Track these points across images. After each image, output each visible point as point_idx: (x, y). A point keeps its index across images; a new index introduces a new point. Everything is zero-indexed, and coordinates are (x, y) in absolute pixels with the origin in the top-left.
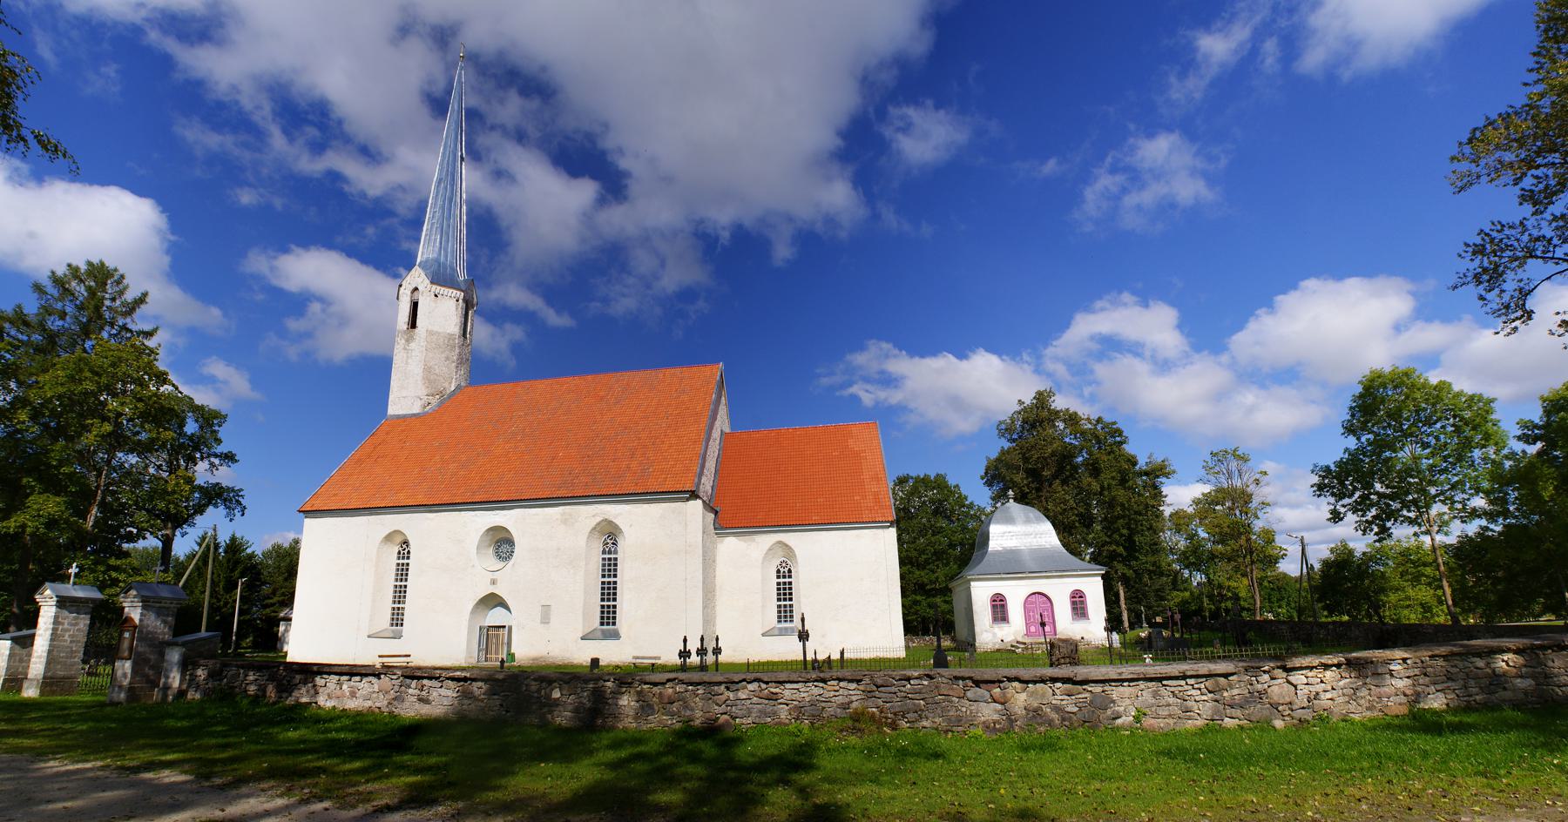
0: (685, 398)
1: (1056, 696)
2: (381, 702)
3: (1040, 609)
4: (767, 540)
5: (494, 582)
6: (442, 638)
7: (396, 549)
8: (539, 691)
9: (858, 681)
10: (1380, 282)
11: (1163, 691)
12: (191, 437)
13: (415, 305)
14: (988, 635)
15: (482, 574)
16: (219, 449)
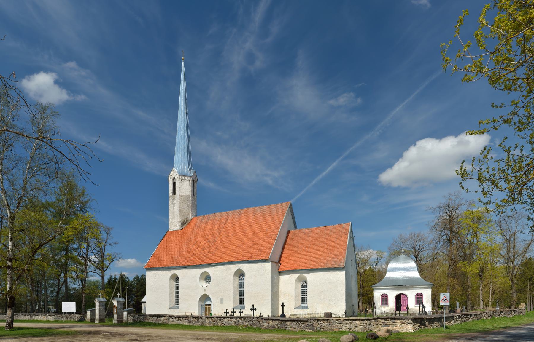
13: (174, 184)
14: (380, 309)
15: (202, 287)
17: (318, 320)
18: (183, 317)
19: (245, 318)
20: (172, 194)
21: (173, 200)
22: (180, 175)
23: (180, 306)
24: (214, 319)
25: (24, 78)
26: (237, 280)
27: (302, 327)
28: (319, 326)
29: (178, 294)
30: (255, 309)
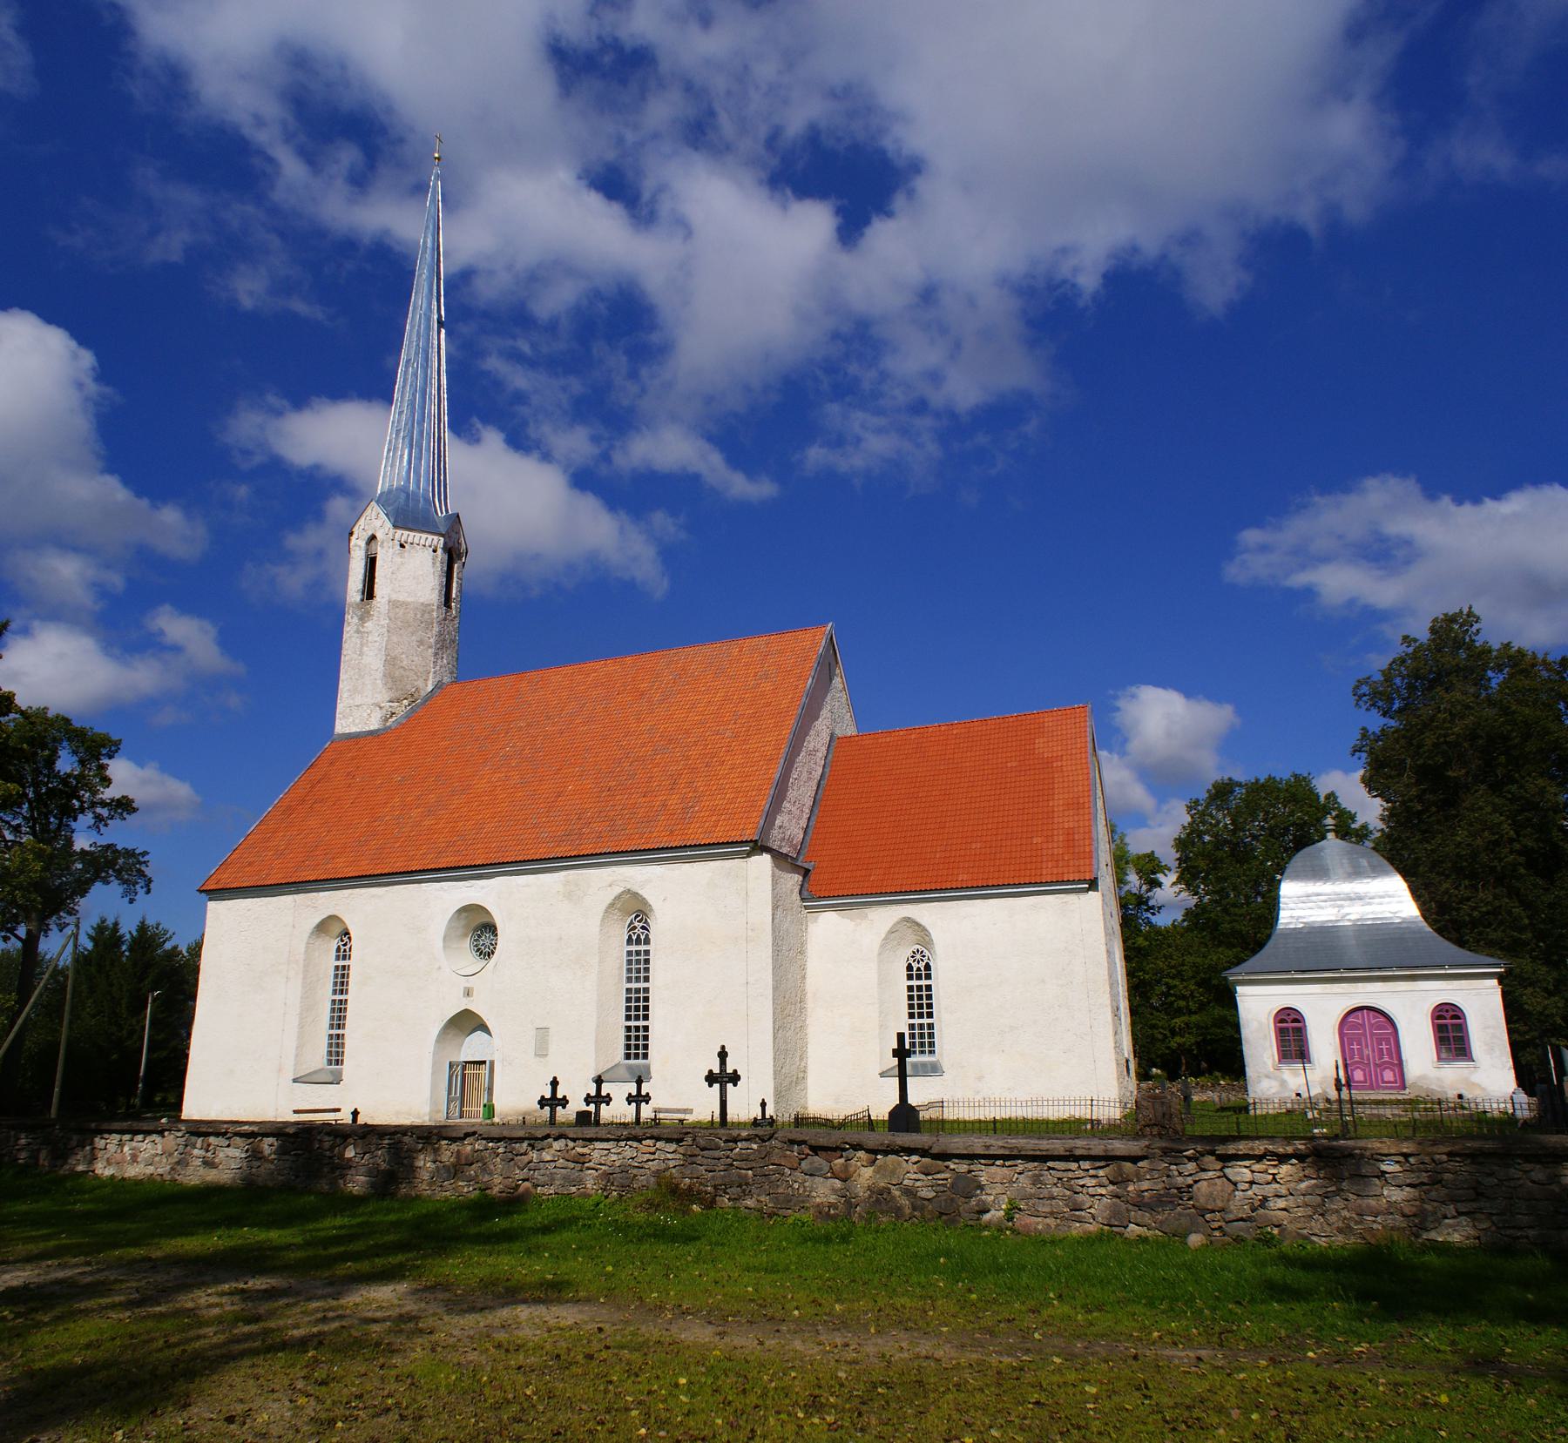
0: (767, 686)
1: (909, 1170)
2: (162, 1168)
3: (1369, 1032)
4: (884, 917)
5: (468, 993)
7: (335, 943)
8: (332, 1148)
9: (679, 1141)
11: (1049, 1178)
12: (65, 780)
13: (371, 563)
14: (1271, 1081)
15: (452, 979)
16: (108, 794)
17: (454, 1140)
20: (358, 598)
21: (363, 619)
23: (347, 1068)
25: (1374, 475)
30: (735, 1078)
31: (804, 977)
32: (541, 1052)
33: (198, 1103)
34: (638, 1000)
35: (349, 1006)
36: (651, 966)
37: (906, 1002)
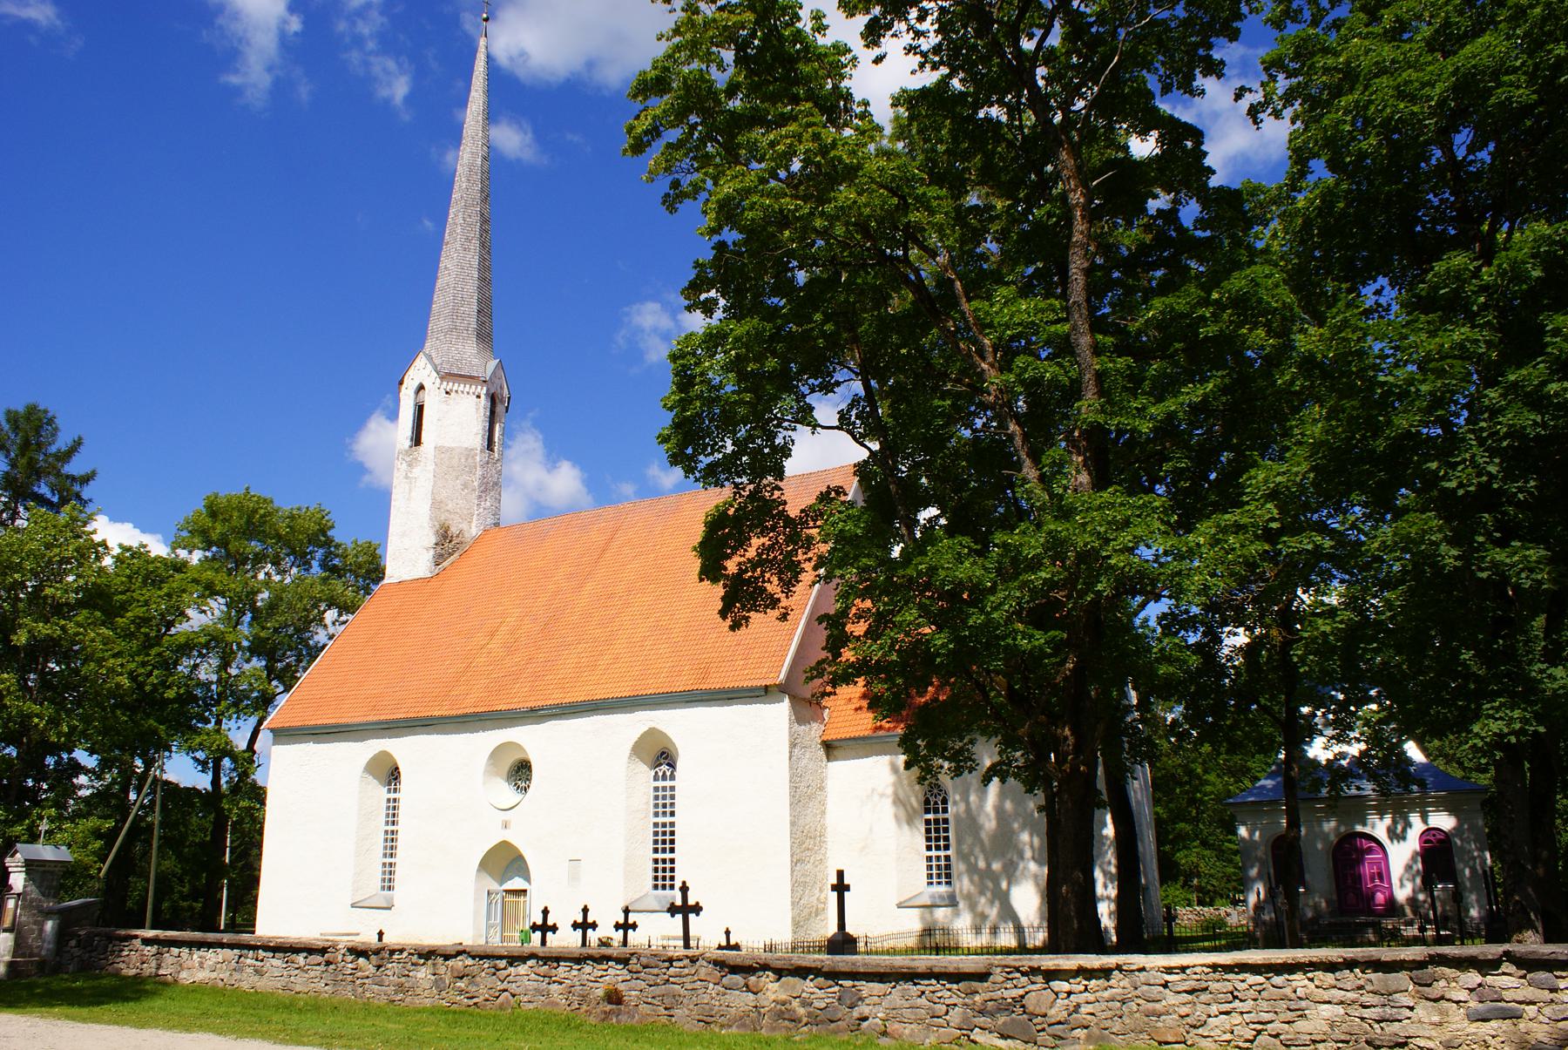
6: (442, 908)
10: (53, 1006)
17: (447, 957)
18: (310, 950)
19: (624, 961)
22: (442, 378)
23: (398, 894)
24: (458, 963)
26: (645, 773)
27: (955, 1016)
28: (1058, 1011)
29: (391, 839)
30: (697, 909)
31: (823, 813)
32: (574, 877)
33: (271, 922)
34: (664, 833)
35: (399, 836)
36: (676, 837)
37: (651, 874)
